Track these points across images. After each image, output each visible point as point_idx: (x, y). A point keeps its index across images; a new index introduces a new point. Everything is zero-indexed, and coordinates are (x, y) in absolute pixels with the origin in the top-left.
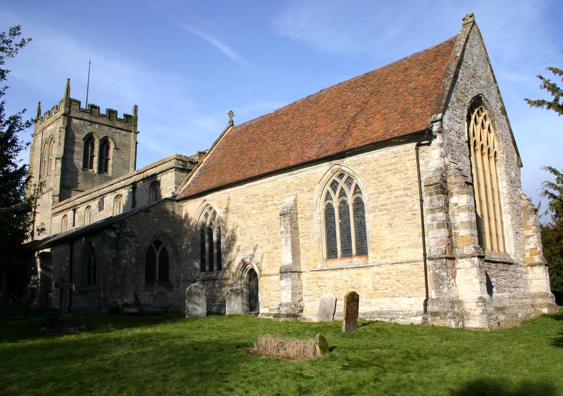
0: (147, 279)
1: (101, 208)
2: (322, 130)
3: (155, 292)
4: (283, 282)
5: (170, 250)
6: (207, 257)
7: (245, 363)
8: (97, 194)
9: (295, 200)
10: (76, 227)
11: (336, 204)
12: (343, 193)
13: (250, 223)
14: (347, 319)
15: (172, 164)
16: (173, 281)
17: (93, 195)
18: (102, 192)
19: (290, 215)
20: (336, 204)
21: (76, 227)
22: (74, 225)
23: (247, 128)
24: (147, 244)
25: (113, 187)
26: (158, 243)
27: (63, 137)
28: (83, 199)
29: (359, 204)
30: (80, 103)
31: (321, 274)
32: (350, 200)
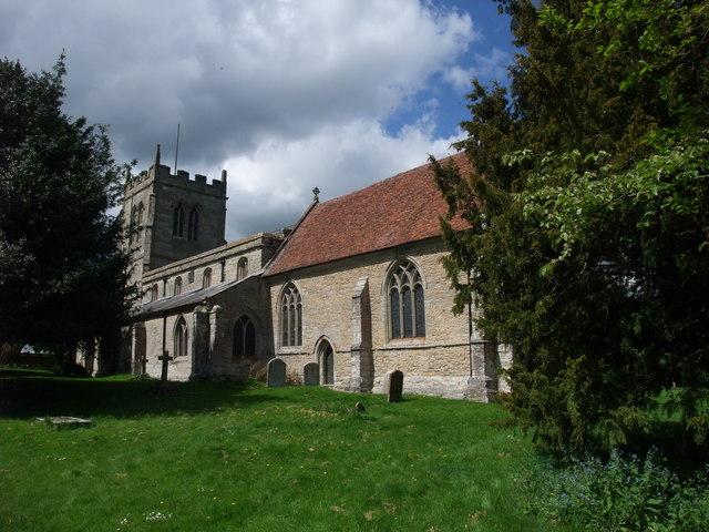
0: (234, 353)
1: (191, 280)
2: (393, 219)
3: (242, 364)
4: (353, 359)
5: (256, 325)
6: (289, 332)
7: (517, 475)
8: (160, 275)
9: (367, 285)
10: (226, 282)
11: (288, 305)
12: (405, 279)
13: (327, 302)
14: (391, 392)
15: (259, 242)
16: (258, 352)
17: (184, 267)
18: (193, 264)
19: (365, 299)
20: (288, 305)
21: (226, 282)
22: (223, 280)
23: (330, 206)
24: (236, 319)
25: (204, 261)
26: (245, 319)
27: (153, 205)
28: (173, 270)
29: (418, 288)
30: (169, 169)
31: (386, 353)
32: (411, 285)
